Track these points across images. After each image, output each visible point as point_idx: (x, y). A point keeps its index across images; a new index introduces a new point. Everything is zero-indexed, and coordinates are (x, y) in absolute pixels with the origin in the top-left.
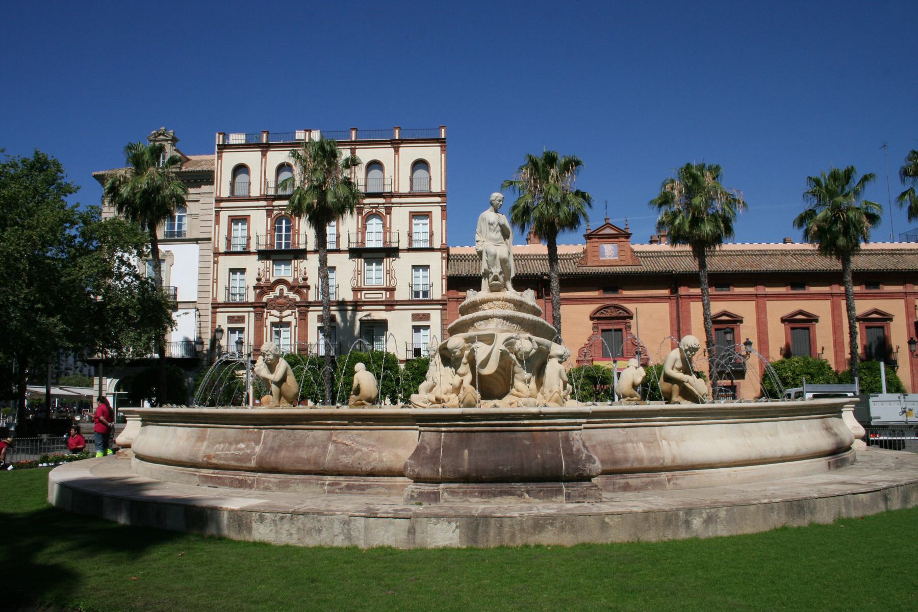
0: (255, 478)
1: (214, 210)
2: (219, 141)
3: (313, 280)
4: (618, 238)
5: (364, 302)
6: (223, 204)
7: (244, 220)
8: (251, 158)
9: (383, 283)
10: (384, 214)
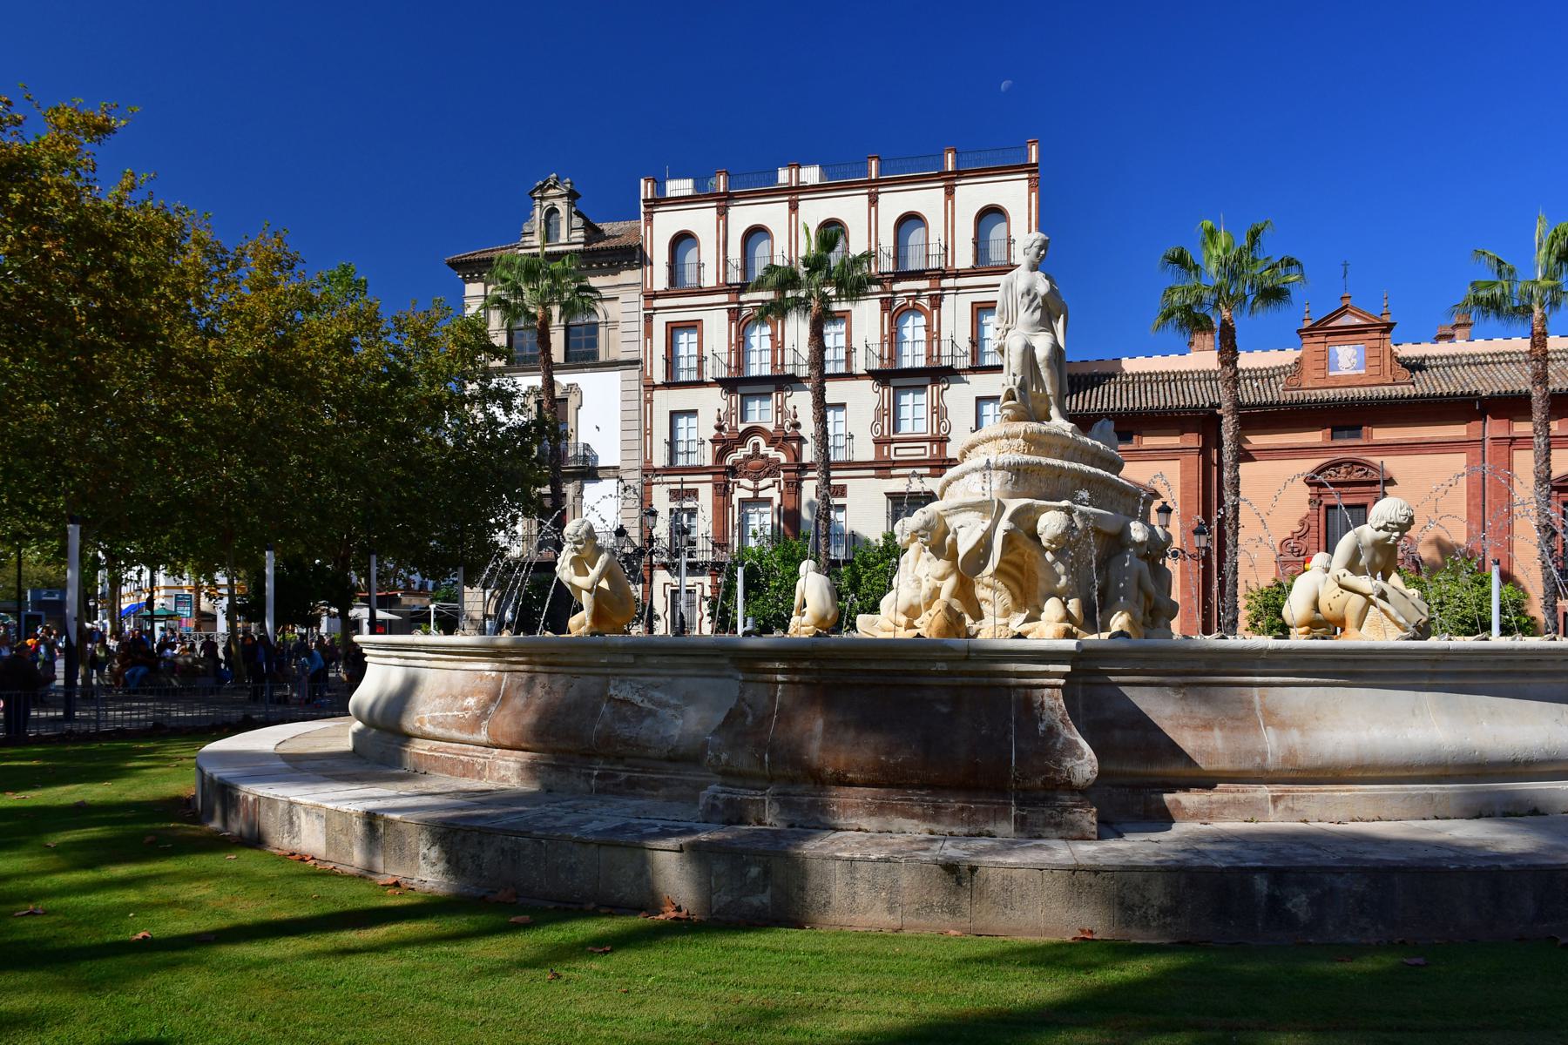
0: (487, 761)
1: (643, 312)
2: (646, 193)
3: (808, 429)
4: (1365, 332)
5: (894, 462)
6: (657, 303)
7: (694, 326)
8: (701, 220)
9: (922, 428)
10: (928, 308)
